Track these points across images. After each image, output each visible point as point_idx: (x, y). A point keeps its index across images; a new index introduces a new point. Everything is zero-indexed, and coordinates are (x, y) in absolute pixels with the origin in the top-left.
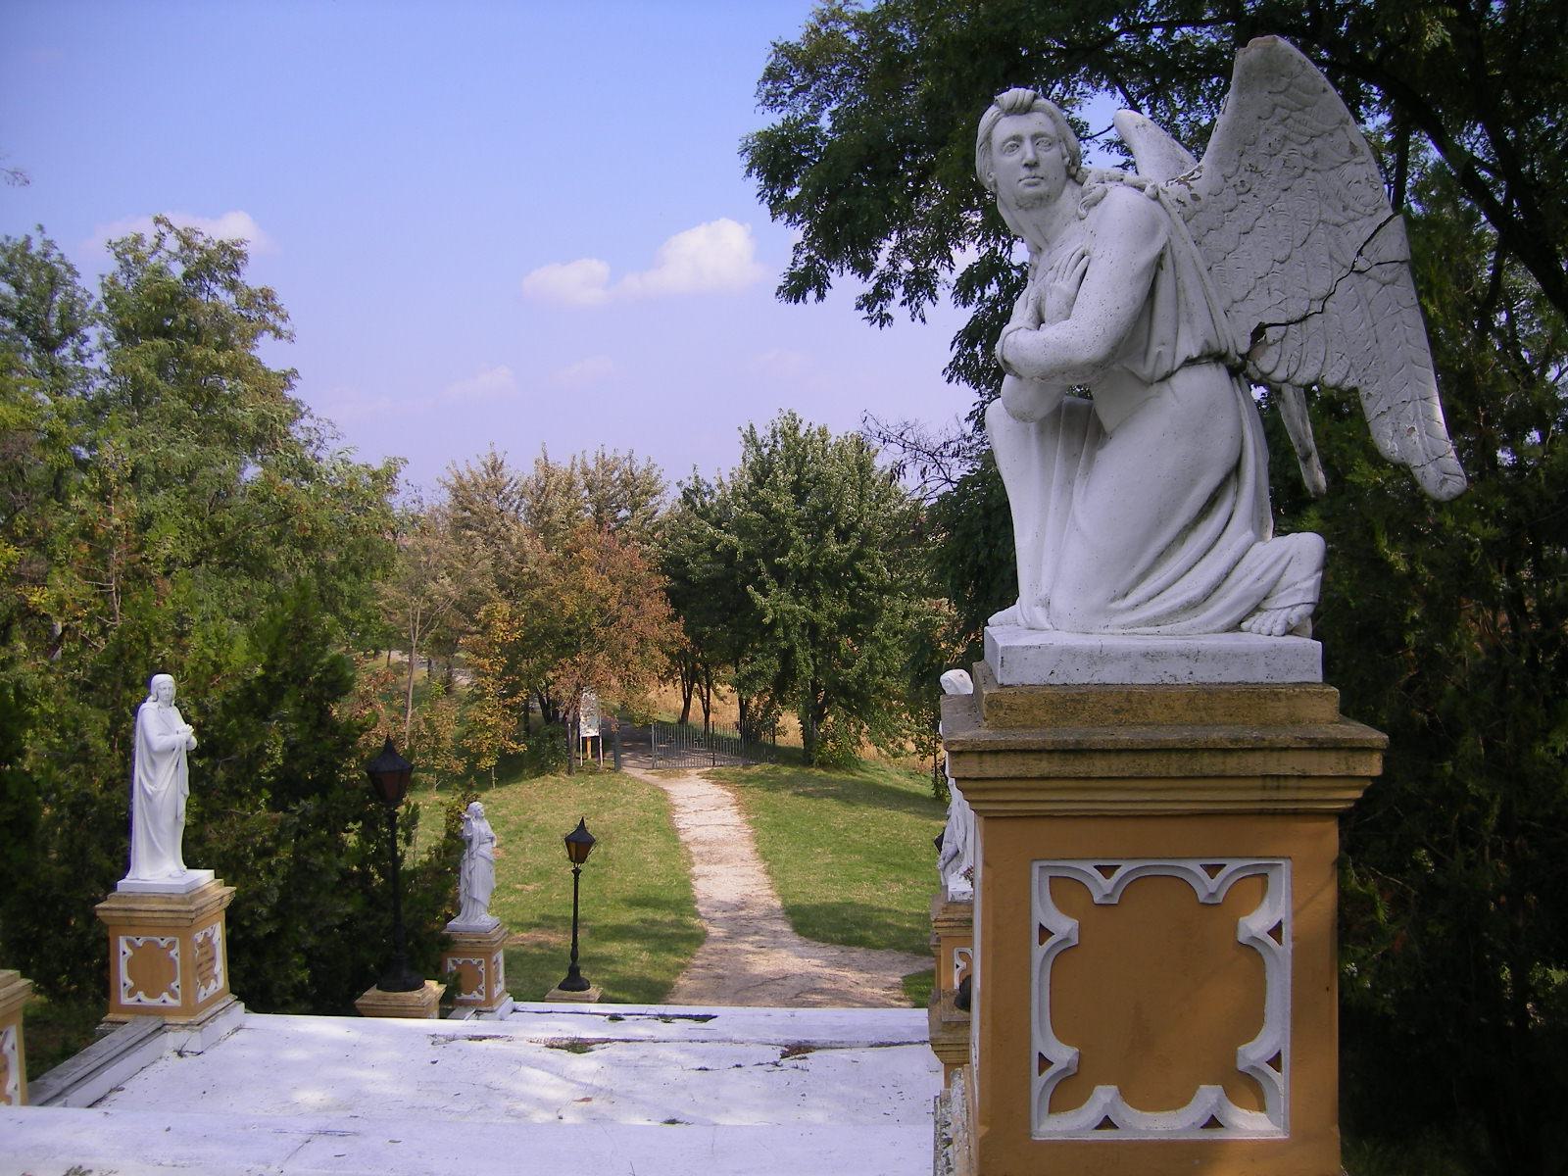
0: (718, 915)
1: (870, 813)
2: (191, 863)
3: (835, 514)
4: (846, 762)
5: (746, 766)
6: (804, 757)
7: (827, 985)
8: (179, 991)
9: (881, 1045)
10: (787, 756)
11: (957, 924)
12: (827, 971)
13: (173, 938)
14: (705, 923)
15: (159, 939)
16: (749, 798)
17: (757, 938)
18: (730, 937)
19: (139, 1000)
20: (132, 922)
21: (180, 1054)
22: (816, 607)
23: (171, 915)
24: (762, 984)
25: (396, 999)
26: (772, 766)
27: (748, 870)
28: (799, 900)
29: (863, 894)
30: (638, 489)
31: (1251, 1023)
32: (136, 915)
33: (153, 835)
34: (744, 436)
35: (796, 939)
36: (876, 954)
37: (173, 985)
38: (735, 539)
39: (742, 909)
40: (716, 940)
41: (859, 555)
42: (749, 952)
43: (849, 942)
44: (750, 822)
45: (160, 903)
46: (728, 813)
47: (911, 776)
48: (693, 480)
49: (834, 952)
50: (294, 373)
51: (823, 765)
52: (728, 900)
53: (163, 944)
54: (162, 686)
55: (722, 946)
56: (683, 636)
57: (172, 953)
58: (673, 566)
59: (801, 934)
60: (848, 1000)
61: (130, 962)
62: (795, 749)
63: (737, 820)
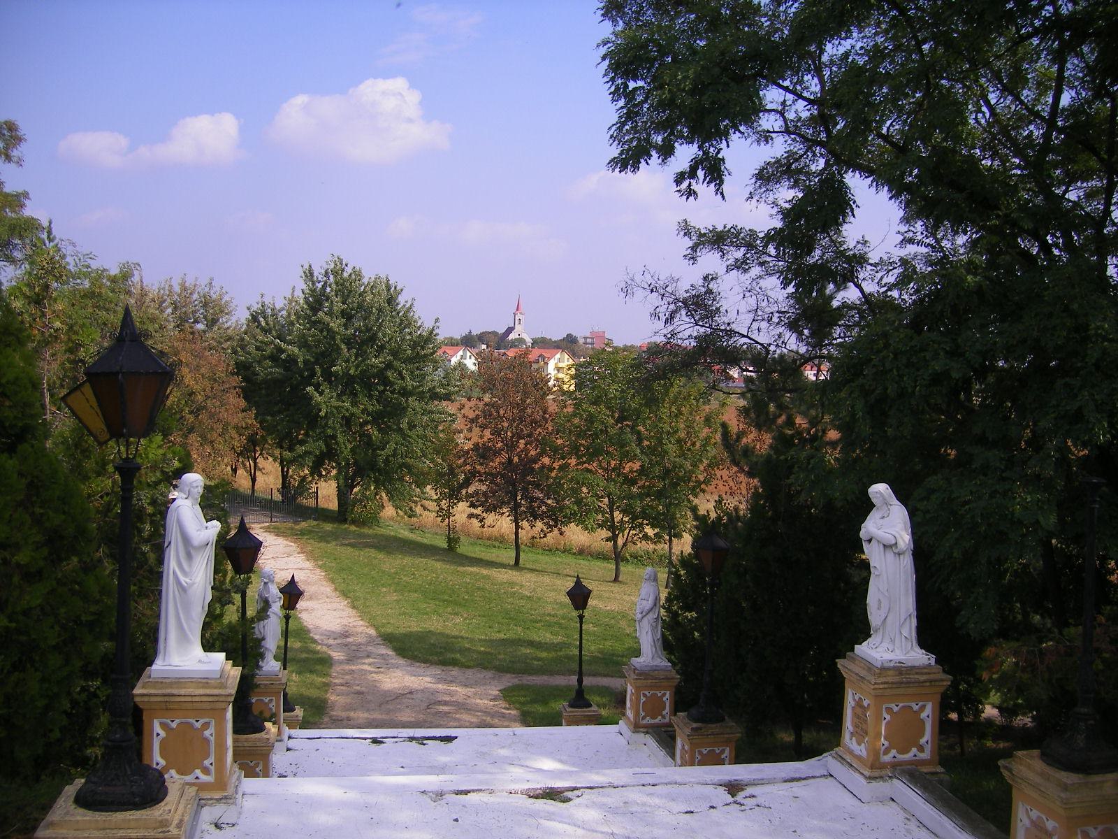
0: (331, 641)
1: (407, 560)
2: (208, 646)
3: (375, 335)
4: (372, 519)
5: (296, 522)
6: (342, 515)
7: (448, 699)
8: (212, 768)
9: (792, 780)
10: (322, 515)
11: (890, 686)
12: (440, 686)
13: (207, 720)
14: (325, 649)
15: (194, 721)
16: (309, 548)
17: (371, 660)
18: (350, 660)
19: (197, 778)
20: (169, 705)
21: (217, 826)
22: (354, 404)
23: (210, 699)
24: (397, 698)
25: (247, 740)
26: (315, 523)
27: (335, 605)
28: (389, 630)
29: (434, 624)
30: (213, 310)
31: (922, 734)
32: (173, 699)
33: (183, 621)
34: (305, 272)
35: (401, 661)
36: (469, 672)
37: (207, 763)
38: (296, 350)
39: (347, 637)
40: (341, 662)
41: (389, 366)
42: (371, 672)
43: (444, 663)
44: (320, 567)
45: (198, 688)
46: (299, 560)
47: (412, 530)
48: (260, 306)
49: (437, 671)
50: (26, 195)
51: (354, 522)
52: (333, 629)
53: (198, 725)
54: (195, 485)
55: (347, 667)
56: (255, 423)
57: (207, 733)
58: (243, 369)
59: (404, 657)
60: (470, 710)
61: (163, 742)
62: (333, 511)
63: (308, 565)
